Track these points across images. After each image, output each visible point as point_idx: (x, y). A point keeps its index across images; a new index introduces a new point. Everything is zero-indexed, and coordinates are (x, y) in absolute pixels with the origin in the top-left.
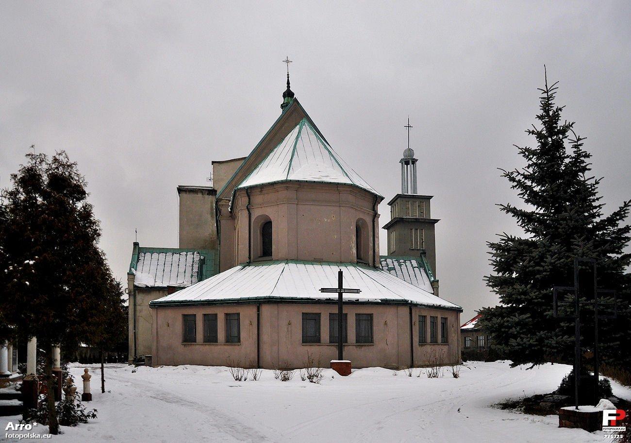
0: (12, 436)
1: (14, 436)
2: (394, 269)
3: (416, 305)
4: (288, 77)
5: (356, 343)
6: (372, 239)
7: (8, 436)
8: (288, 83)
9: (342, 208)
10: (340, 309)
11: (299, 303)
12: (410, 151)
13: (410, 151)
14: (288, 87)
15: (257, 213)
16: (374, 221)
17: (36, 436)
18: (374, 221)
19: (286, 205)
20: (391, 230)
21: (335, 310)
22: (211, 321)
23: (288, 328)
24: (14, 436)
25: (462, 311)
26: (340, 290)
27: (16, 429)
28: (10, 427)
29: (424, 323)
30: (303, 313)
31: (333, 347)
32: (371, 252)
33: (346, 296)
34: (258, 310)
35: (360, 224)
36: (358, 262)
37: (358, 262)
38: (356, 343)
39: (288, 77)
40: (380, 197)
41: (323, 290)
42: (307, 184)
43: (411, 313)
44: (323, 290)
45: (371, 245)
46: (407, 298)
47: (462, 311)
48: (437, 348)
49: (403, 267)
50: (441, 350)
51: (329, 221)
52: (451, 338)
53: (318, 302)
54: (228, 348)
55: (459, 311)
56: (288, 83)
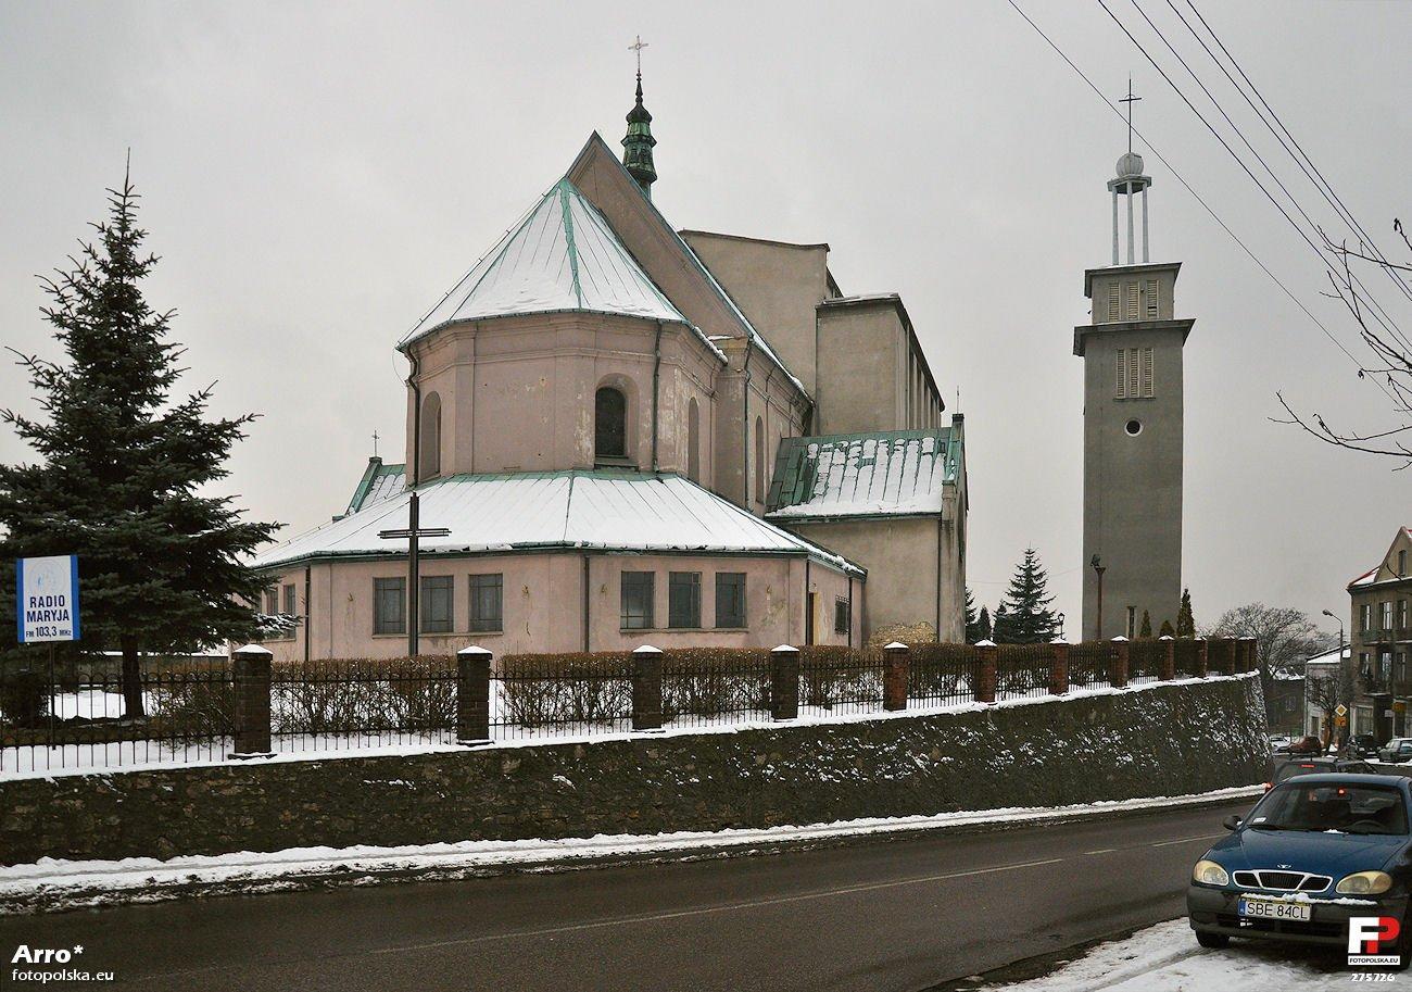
0: (28, 976)
1: (32, 977)
2: (873, 462)
3: (603, 552)
4: (639, 80)
5: (470, 631)
6: (649, 412)
7: (17, 975)
8: (639, 93)
9: (561, 360)
12: (1132, 160)
13: (1132, 160)
14: (639, 100)
17: (81, 976)
19: (454, 369)
22: (12, 596)
23: (348, 609)
24: (32, 977)
26: (414, 531)
27: (37, 960)
28: (23, 956)
30: (376, 580)
33: (425, 543)
36: (597, 467)
37: (597, 467)
39: (639, 80)
41: (385, 535)
42: (491, 322)
43: (587, 568)
44: (385, 535)
45: (648, 426)
46: (568, 539)
49: (898, 456)
56: (639, 93)
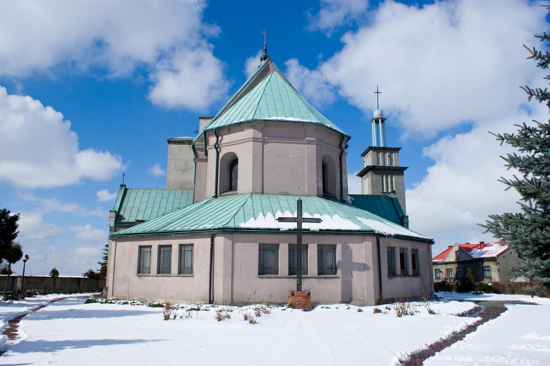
5: (318, 275)
6: (338, 174)
10: (299, 239)
11: (256, 233)
15: (224, 151)
16: (340, 158)
18: (340, 158)
20: (364, 177)
21: (294, 239)
25: (433, 243)
26: (299, 220)
29: (393, 254)
31: (292, 280)
32: (338, 187)
33: (305, 226)
34: (212, 241)
35: (327, 160)
38: (318, 275)
40: (346, 136)
45: (338, 180)
47: (433, 243)
48: (407, 279)
50: (413, 283)
51: (294, 157)
52: (468, 355)
53: (276, 231)
54: (181, 280)
55: (430, 242)
